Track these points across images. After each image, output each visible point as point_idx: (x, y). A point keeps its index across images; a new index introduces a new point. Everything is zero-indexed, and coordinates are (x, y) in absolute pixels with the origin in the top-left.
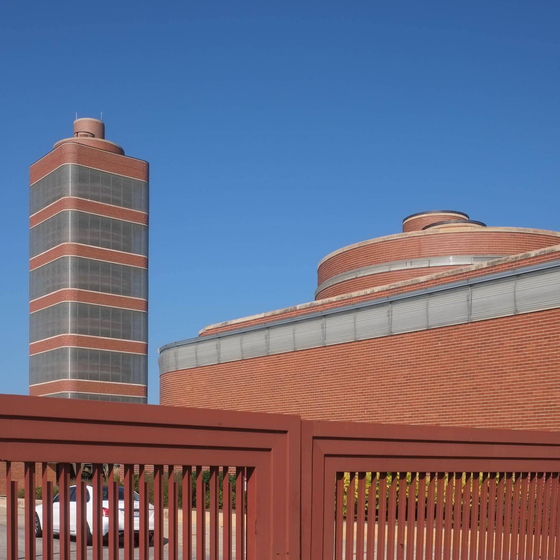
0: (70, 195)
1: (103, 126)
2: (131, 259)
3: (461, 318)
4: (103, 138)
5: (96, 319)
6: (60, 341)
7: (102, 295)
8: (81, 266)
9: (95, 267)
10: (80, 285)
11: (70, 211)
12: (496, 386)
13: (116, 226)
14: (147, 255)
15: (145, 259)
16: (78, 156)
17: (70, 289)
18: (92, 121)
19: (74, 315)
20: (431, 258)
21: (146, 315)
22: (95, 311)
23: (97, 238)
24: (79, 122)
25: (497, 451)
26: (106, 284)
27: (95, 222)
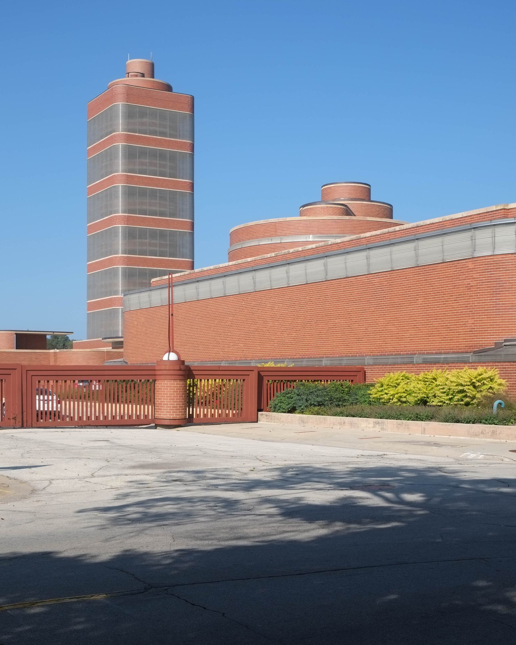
0: (120, 131)
1: (152, 65)
2: (176, 185)
4: (153, 77)
6: (111, 262)
7: (150, 218)
8: (130, 193)
9: (143, 193)
11: (120, 145)
12: (264, 329)
13: (162, 155)
14: (193, 180)
16: (127, 96)
17: (120, 214)
18: (142, 62)
20: (282, 237)
21: (192, 234)
22: (143, 233)
23: (145, 167)
24: (131, 63)
26: (154, 208)
27: (143, 153)
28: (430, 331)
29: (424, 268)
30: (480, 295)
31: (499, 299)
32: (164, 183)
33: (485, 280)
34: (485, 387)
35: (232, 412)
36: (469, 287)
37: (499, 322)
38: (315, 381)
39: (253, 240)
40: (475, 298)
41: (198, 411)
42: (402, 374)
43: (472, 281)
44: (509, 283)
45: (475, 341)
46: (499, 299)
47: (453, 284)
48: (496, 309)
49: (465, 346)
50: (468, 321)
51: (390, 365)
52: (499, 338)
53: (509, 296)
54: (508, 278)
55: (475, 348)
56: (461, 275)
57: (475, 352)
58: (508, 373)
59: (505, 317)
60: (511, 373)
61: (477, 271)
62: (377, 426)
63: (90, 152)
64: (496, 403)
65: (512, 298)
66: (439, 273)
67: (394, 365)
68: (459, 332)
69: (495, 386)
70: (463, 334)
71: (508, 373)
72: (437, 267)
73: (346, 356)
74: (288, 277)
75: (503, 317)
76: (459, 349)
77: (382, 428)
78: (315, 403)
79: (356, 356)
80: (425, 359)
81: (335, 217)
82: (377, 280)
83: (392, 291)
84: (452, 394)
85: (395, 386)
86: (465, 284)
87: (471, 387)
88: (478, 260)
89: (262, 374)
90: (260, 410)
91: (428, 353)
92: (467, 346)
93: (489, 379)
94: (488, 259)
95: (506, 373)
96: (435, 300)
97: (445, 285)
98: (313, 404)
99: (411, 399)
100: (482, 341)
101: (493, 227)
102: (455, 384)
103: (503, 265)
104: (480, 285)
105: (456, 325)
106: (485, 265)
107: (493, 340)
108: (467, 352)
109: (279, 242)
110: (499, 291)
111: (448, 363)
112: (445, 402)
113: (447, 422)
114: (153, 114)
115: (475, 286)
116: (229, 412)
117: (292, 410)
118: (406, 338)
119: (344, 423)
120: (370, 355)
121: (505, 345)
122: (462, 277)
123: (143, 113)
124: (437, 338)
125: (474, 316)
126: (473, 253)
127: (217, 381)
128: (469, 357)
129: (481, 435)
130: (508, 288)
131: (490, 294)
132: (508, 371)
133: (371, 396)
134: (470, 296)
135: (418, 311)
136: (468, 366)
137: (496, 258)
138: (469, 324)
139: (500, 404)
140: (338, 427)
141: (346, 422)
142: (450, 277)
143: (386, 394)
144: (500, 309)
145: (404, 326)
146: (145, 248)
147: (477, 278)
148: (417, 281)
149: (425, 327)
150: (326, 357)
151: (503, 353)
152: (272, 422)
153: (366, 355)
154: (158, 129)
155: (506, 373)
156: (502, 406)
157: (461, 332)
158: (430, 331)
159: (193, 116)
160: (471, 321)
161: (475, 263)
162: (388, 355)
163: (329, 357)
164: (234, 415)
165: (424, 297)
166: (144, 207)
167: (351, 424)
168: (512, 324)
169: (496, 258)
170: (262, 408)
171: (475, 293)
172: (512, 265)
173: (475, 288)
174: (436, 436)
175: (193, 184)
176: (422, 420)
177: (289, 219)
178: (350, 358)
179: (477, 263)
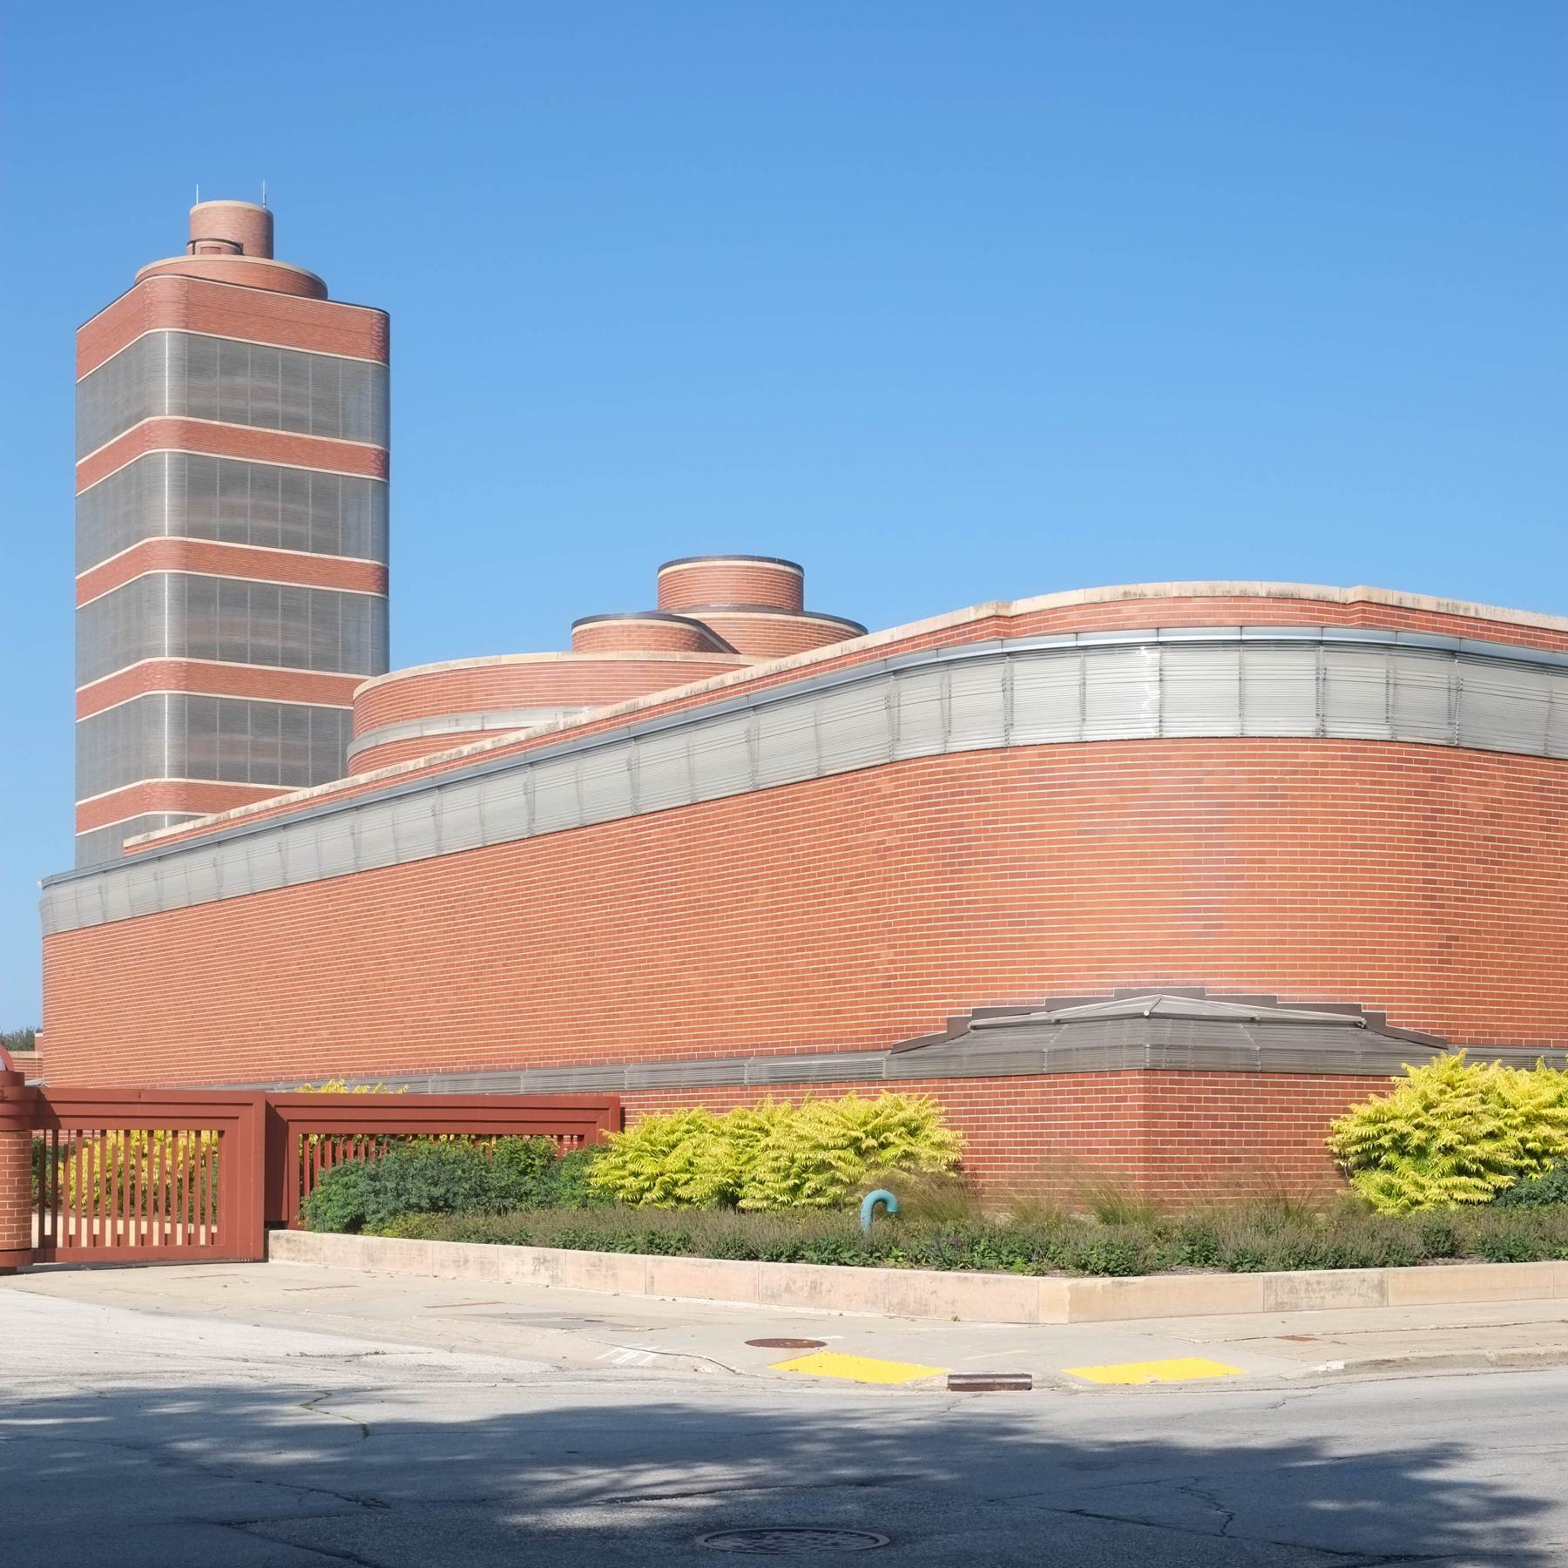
0: (166, 408)
1: (268, 220)
3: (518, 829)
5: (238, 737)
8: (195, 596)
9: (234, 596)
10: (191, 647)
11: (166, 453)
13: (292, 485)
14: (386, 559)
15: (379, 568)
16: (187, 308)
17: (167, 659)
18: (236, 209)
19: (178, 725)
20: (485, 713)
22: (232, 717)
23: (239, 521)
25: (480, 1115)
27: (234, 478)
28: (787, 987)
29: (771, 797)
30: (909, 876)
31: (960, 887)
32: (299, 567)
33: (923, 829)
34: (888, 1153)
35: (208, 1230)
36: (882, 851)
37: (959, 957)
38: (479, 1137)
39: (406, 723)
40: (896, 885)
41: (67, 1226)
42: (690, 1116)
43: (889, 834)
44: (986, 838)
45: (896, 1015)
46: (960, 887)
47: (842, 842)
48: (952, 919)
49: (874, 1032)
50: (877, 956)
51: (685, 1090)
52: (959, 1005)
53: (986, 878)
54: (985, 823)
55: (896, 1037)
56: (861, 816)
57: (897, 1049)
58: (979, 1112)
59: (977, 941)
60: (983, 1112)
61: (903, 801)
62: (542, 1268)
63: (85, 474)
64: (869, 1199)
65: (996, 885)
66: (808, 811)
67: (695, 1088)
68: (855, 988)
69: (922, 1149)
70: (868, 995)
71: (979, 1112)
72: (804, 790)
73: (579, 1065)
74: (438, 828)
75: (969, 941)
76: (858, 1040)
77: (552, 1277)
78: (425, 1203)
79: (602, 1063)
80: (772, 1069)
81: (642, 655)
82: (656, 834)
83: (693, 867)
84: (798, 1176)
85: (663, 1152)
86: (871, 844)
87: (850, 1154)
88: (904, 770)
89: (284, 1114)
90: (275, 1220)
91: (781, 1054)
92: (877, 1031)
93: (903, 1129)
94: (931, 766)
95: (971, 1112)
96: (799, 892)
97: (824, 845)
98: (418, 1205)
99: (698, 1189)
100: (914, 1014)
101: (944, 668)
102: (808, 1145)
103: (971, 785)
104: (910, 846)
105: (850, 966)
106: (923, 783)
107: (944, 1013)
108: (877, 1050)
109: (478, 728)
110: (960, 864)
111: (827, 1084)
112: (775, 1200)
113: (720, 1256)
114: (266, 363)
115: (897, 847)
116: (174, 1229)
117: (354, 1226)
118: (726, 1007)
119: (466, 1261)
120: (637, 1061)
121: (974, 1028)
122: (866, 823)
123: (234, 362)
124: (802, 1008)
125: (895, 939)
126: (892, 748)
127: (205, 1135)
128: (878, 1064)
129: (786, 1296)
130: (984, 854)
131: (937, 873)
132: (977, 1104)
133: (592, 1181)
134: (885, 879)
135: (758, 927)
136: (858, 1092)
137: (952, 764)
138: (882, 963)
139: (883, 1201)
140: (449, 1273)
141: (471, 1258)
142: (836, 821)
143: (636, 1175)
144: (961, 918)
145: (722, 973)
146: (240, 759)
147: (903, 824)
148: (754, 836)
149: (772, 975)
150: (532, 1067)
151: (965, 1051)
152: (309, 1257)
153: (629, 1061)
154: (279, 408)
155: (971, 1112)
156: (890, 1209)
157: (861, 988)
158: (787, 987)
159: (387, 371)
160: (886, 955)
161: (897, 779)
162: (683, 1059)
163: (538, 1067)
164: (212, 1238)
165: (771, 882)
166: (239, 639)
167: (482, 1264)
168: (995, 964)
169: (952, 764)
170: (284, 1218)
171: (896, 870)
172: (995, 783)
173: (896, 855)
174: (679, 1300)
175: (385, 572)
176: (666, 1253)
177: (505, 659)
178: (587, 1070)
179: (904, 778)
